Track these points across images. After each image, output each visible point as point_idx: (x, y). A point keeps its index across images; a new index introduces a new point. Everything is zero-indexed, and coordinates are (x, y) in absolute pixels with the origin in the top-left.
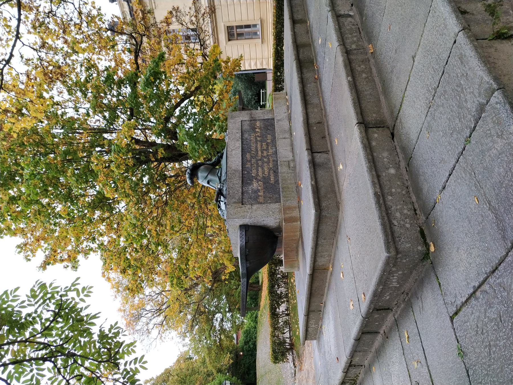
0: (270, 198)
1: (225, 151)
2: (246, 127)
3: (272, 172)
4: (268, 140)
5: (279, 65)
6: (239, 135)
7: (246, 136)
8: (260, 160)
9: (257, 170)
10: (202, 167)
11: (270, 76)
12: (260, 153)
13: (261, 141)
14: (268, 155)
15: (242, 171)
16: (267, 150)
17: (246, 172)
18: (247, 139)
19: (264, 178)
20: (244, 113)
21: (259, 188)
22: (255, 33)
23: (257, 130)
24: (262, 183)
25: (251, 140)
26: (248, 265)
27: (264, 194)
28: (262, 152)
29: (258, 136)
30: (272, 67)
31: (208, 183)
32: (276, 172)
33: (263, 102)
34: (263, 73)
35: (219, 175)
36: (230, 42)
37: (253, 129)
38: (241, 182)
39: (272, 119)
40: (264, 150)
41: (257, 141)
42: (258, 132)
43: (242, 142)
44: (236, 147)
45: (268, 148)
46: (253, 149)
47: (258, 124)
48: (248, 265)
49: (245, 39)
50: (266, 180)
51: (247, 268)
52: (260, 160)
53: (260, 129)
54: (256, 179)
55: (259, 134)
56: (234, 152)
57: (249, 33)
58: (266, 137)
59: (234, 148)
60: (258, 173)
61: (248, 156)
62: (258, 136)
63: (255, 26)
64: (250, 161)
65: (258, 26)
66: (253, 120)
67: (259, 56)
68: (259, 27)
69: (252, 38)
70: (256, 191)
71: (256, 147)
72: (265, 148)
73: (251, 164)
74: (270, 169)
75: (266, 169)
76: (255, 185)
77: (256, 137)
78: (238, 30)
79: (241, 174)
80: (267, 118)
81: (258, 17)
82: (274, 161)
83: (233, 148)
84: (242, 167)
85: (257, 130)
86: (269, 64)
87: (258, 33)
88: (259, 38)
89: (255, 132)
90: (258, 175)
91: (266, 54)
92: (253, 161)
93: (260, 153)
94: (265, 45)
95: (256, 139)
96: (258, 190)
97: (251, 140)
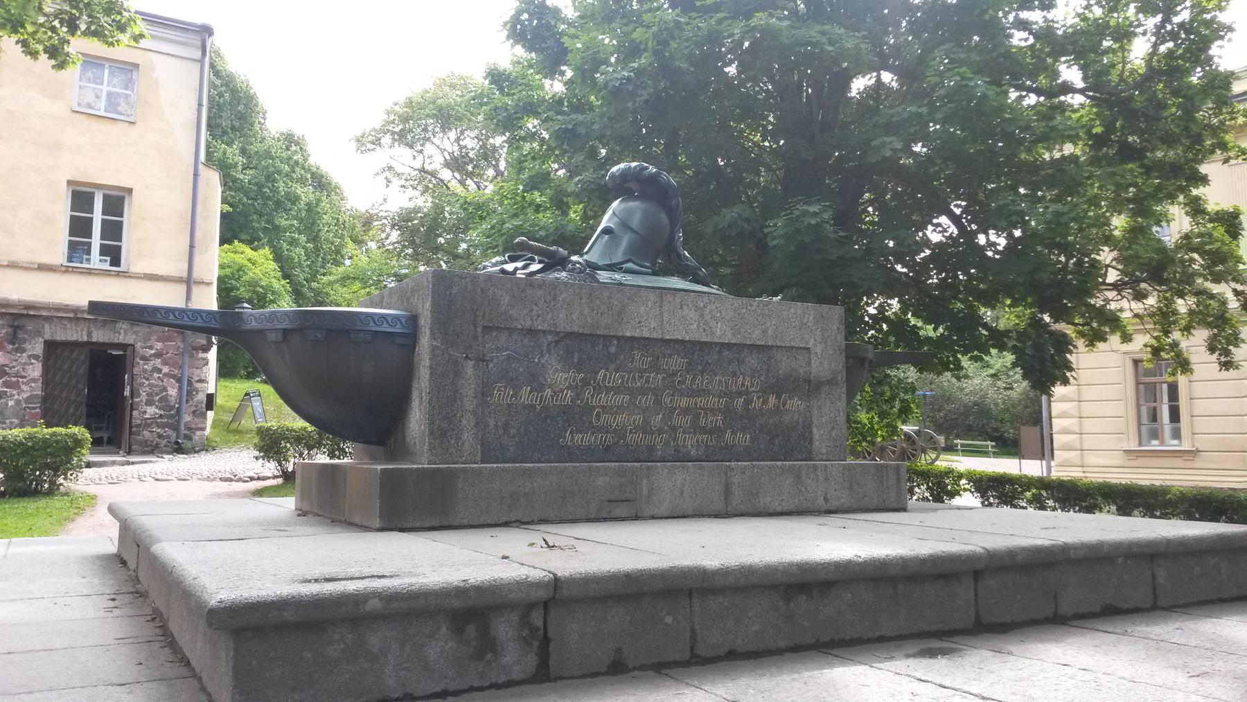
0: (506, 427)
1: (714, 290)
2: (784, 364)
3: (610, 438)
4: (733, 433)
5: (1075, 496)
6: (756, 337)
7: (753, 361)
8: (658, 402)
9: (618, 390)
10: (664, 218)
11: (1032, 468)
12: (684, 402)
13: (728, 411)
14: (673, 429)
15: (618, 338)
16: (696, 428)
17: (612, 350)
18: (741, 362)
19: (587, 410)
20: (839, 364)
21: (548, 392)
22: (1155, 434)
23: (772, 400)
24: (568, 401)
25: (734, 374)
26: (272, 337)
27: (524, 406)
28: (686, 411)
29: (748, 402)
30: (1055, 474)
31: (607, 231)
32: (605, 453)
33: (962, 445)
34: (1044, 450)
35: (630, 265)
36: (1130, 366)
37: (781, 386)
38: (576, 329)
39: (811, 452)
40: (697, 417)
41: (732, 395)
42: (765, 402)
43: (729, 346)
44: (713, 323)
45: (703, 430)
46: (702, 382)
47: (795, 404)
48: (272, 337)
49: (1138, 406)
50: (577, 416)
51: (261, 332)
52: (658, 402)
53: (777, 407)
54: (585, 383)
55: (757, 403)
56: (693, 315)
57: (1154, 417)
58: (744, 429)
59: (708, 317)
60: (608, 390)
61: (676, 362)
62: (748, 402)
63: (1177, 434)
64: (654, 367)
65: (1176, 442)
66: (812, 387)
67: (1089, 442)
68: (1173, 445)
69: (1140, 424)
70: (535, 381)
71: (704, 392)
72: (702, 422)
73: (642, 371)
74: (620, 433)
75: (619, 418)
76: (558, 377)
77: (747, 393)
78: (1165, 387)
79: (606, 332)
80: (816, 435)
81: (1199, 445)
82: (651, 449)
83: (707, 312)
84: (633, 338)
85: (772, 400)
86: (1064, 466)
87: (1155, 442)
88: (1140, 444)
89: (764, 393)
90: (599, 389)
91: (1091, 459)
92: (656, 379)
93: (684, 402)
94: (1119, 459)
95: (740, 394)
96: (540, 388)
97: (734, 374)
